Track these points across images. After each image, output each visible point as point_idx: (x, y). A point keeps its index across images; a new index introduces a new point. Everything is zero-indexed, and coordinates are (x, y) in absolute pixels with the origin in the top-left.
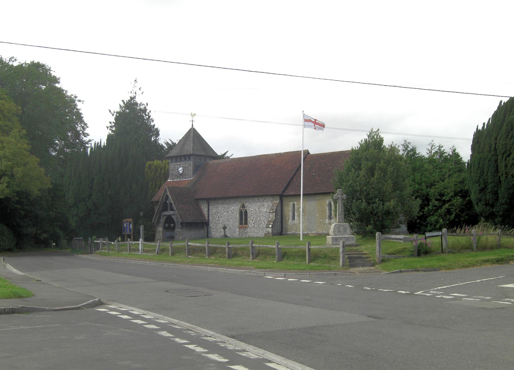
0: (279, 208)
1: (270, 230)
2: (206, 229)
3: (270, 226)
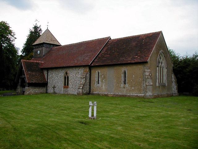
0: (88, 75)
1: (81, 90)
2: (46, 88)
3: (81, 88)
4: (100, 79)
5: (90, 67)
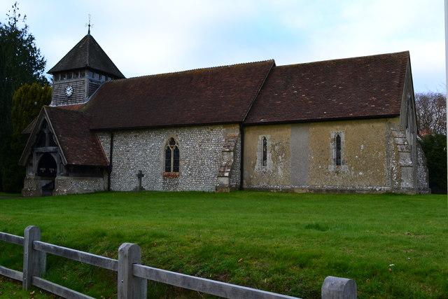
0: (239, 145)
3: (227, 174)
4: (269, 155)
5: (244, 126)
